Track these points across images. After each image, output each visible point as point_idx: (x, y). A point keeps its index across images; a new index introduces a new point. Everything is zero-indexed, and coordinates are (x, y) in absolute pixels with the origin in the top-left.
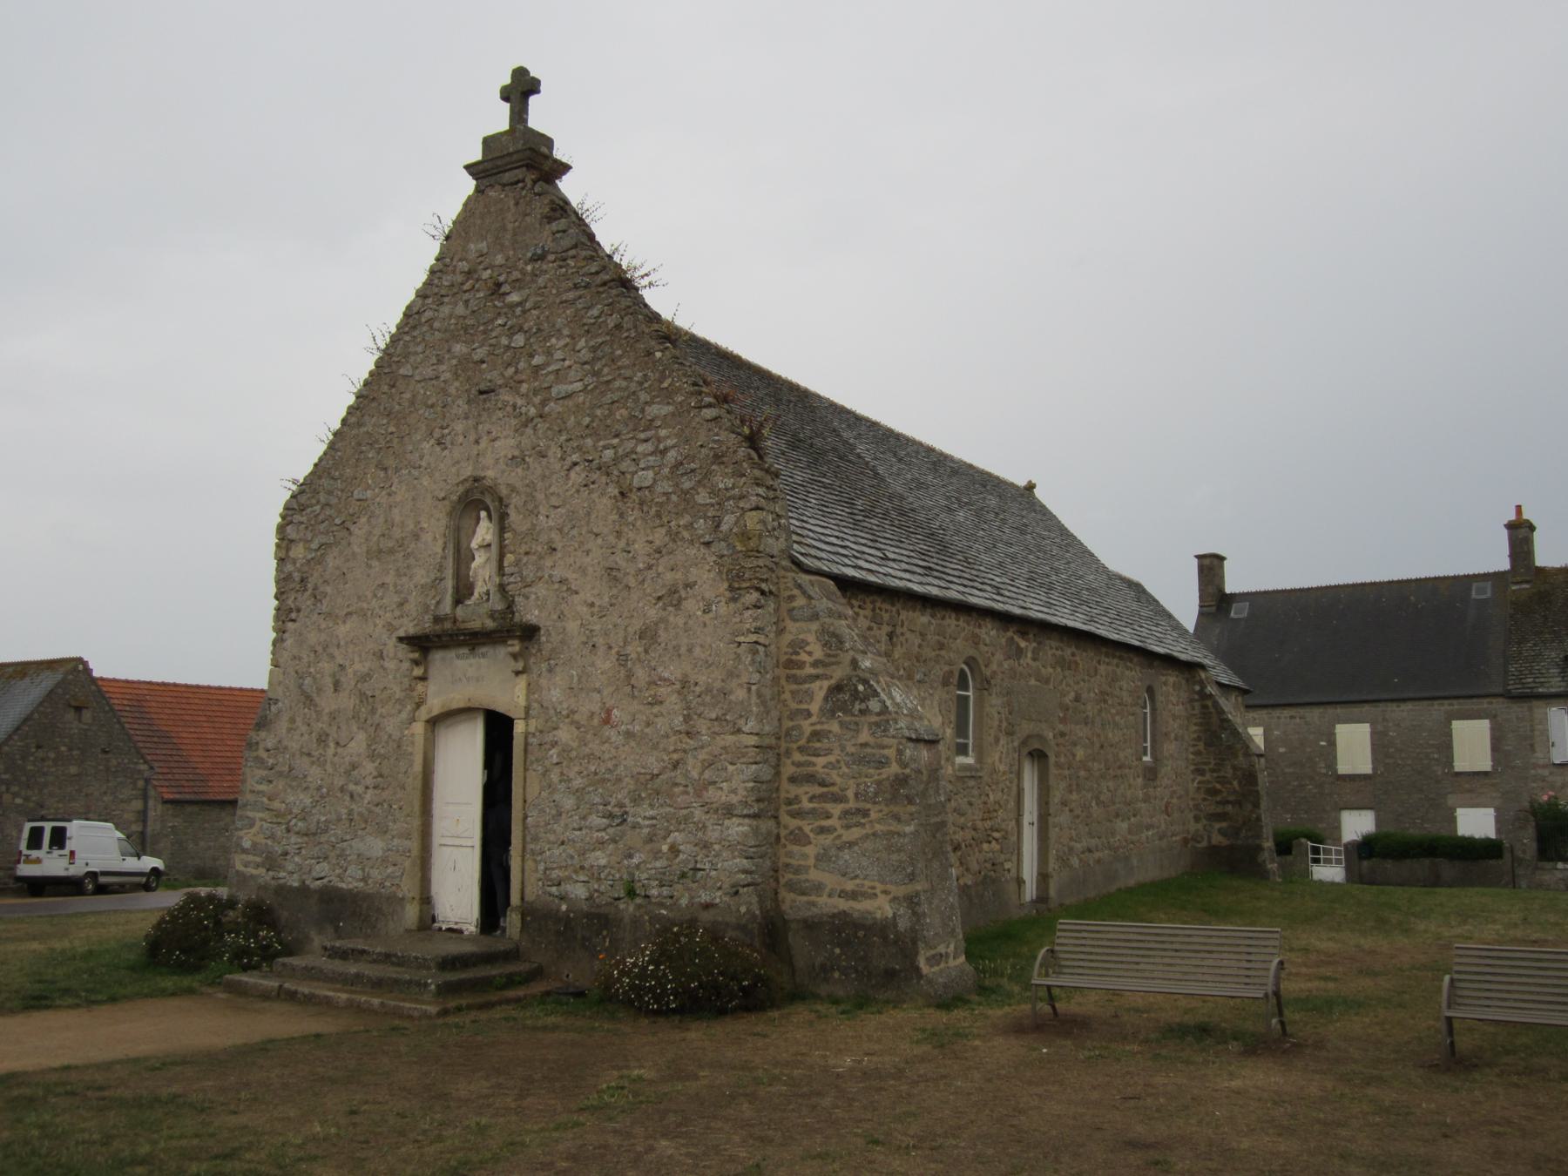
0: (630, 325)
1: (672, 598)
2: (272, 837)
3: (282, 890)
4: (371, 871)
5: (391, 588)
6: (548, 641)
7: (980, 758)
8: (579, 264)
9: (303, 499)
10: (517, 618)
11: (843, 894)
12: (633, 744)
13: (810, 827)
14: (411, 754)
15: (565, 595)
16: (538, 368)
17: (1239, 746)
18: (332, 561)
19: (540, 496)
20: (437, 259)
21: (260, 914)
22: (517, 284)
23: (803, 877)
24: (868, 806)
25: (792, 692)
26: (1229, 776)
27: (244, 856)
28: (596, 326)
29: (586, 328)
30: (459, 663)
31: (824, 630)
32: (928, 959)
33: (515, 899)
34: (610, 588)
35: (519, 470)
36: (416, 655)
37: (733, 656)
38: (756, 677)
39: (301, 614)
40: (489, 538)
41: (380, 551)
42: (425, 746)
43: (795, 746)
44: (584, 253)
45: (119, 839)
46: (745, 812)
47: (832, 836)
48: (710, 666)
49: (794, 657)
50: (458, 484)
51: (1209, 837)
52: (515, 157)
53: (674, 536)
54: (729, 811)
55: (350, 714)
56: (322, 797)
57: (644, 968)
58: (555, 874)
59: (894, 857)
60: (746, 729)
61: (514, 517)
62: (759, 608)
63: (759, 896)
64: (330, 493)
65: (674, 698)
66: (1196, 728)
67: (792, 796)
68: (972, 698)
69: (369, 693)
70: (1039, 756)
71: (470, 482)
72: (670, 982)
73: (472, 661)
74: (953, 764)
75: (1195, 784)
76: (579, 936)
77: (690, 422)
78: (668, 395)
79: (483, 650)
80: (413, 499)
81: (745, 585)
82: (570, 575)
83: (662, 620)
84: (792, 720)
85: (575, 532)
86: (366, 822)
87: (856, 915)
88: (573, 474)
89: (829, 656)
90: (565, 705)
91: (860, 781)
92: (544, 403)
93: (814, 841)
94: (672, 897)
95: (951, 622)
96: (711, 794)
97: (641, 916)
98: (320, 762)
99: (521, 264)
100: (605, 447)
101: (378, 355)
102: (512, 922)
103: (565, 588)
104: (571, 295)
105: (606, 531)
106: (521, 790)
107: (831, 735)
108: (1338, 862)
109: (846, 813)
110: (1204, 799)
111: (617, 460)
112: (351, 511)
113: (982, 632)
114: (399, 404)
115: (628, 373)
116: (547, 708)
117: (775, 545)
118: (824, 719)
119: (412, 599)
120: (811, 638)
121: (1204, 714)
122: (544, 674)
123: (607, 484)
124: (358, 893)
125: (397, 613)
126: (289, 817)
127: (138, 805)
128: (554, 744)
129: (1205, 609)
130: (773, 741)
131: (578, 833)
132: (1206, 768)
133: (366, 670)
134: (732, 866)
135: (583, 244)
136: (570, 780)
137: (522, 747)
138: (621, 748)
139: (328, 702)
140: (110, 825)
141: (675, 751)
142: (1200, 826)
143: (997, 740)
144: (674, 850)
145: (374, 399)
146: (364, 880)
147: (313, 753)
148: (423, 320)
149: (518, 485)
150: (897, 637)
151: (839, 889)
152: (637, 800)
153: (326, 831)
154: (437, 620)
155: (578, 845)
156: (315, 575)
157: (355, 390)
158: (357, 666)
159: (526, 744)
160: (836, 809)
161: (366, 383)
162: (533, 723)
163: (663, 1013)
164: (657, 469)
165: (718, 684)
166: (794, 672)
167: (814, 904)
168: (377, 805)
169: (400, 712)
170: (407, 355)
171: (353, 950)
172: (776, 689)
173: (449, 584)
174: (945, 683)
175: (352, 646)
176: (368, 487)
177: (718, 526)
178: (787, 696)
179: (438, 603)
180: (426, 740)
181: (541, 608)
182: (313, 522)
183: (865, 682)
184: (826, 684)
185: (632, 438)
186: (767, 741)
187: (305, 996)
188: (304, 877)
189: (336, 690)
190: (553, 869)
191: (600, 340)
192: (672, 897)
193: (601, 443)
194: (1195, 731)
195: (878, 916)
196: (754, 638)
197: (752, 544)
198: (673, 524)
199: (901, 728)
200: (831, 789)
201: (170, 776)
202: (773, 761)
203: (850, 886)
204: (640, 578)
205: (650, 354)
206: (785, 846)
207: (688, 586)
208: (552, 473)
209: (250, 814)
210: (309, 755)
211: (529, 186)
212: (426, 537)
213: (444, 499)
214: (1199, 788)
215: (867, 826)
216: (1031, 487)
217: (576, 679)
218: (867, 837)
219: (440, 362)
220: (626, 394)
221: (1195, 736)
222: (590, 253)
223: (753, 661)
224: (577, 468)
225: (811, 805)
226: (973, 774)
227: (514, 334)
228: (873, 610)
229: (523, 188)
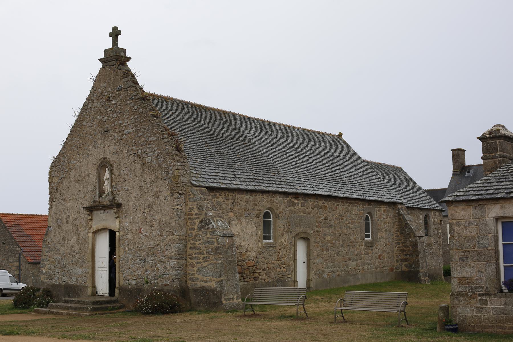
0: (145, 112)
1: (156, 195)
2: (50, 269)
3: (54, 286)
4: (78, 278)
5: (82, 192)
6: (124, 208)
7: (275, 240)
8: (131, 92)
9: (56, 163)
10: (116, 202)
11: (204, 281)
12: (147, 239)
14: (88, 243)
16: (120, 125)
17: (412, 233)
18: (65, 183)
19: (121, 164)
20: (92, 88)
21: (47, 293)
22: (115, 98)
23: (193, 277)
24: (209, 256)
25: (190, 223)
26: (408, 244)
27: (43, 276)
28: (136, 112)
29: (133, 112)
30: (101, 215)
31: (198, 205)
32: (225, 299)
33: (117, 285)
34: (141, 192)
35: (116, 156)
36: (89, 213)
37: (172, 213)
38: (178, 219)
39: (57, 200)
40: (108, 176)
41: (78, 180)
42: (92, 240)
43: (191, 238)
44: (132, 89)
45: (10, 276)
46: (175, 258)
47: (200, 265)
49: (190, 212)
50: (99, 160)
51: (402, 268)
52: (113, 58)
53: (157, 177)
54: (171, 258)
55: (71, 231)
56: (64, 256)
57: (144, 301)
58: (127, 277)
59: (216, 270)
60: (175, 234)
61: (115, 171)
62: (179, 198)
63: (179, 282)
64: (64, 161)
65: (157, 225)
66: (397, 227)
67: (190, 253)
68: (272, 220)
69: (77, 224)
70: (306, 239)
71: (103, 159)
72: (150, 305)
73: (105, 214)
74: (262, 242)
75: (397, 248)
76: (134, 295)
77: (161, 143)
78: (155, 134)
79: (107, 211)
80: (87, 164)
81: (175, 192)
82: (130, 189)
83: (154, 202)
84: (190, 231)
85: (131, 175)
86: (77, 264)
87: (206, 287)
88: (130, 158)
89: (199, 212)
90: (129, 227)
91: (207, 248)
92: (122, 135)
93: (196, 266)
94: (157, 283)
95: (260, 197)
96: (168, 253)
97: (150, 289)
98: (63, 246)
100: (139, 150)
101: (77, 118)
102: (117, 291)
103: (129, 192)
104: (129, 102)
105: (139, 175)
106: (118, 253)
107: (200, 235)
109: (204, 258)
110: (400, 254)
111: (142, 153)
112: (70, 168)
113: (275, 199)
114: (83, 134)
115: (144, 127)
117: (185, 179)
119: (87, 195)
120: (195, 207)
121: (400, 221)
122: (123, 218)
123: (139, 161)
124: (75, 285)
125: (84, 200)
126: (55, 263)
127: (17, 264)
128: (127, 239)
129: (455, 173)
130: (184, 237)
131: (133, 265)
132: (401, 242)
133: (75, 217)
134: (172, 274)
135: (132, 86)
136: (131, 250)
137: (118, 240)
138: (144, 240)
139: (65, 227)
140: (6, 271)
141: (158, 240)
142: (398, 264)
143: (283, 234)
144: (158, 269)
145: (76, 132)
146: (76, 281)
147: (61, 243)
148: (89, 107)
149: (116, 160)
150: (236, 203)
151: (202, 280)
152: (148, 255)
153: (66, 267)
154: (95, 202)
155: (133, 269)
156: (60, 187)
157: (70, 129)
158: (73, 216)
159: (119, 239)
160: (201, 257)
161: (73, 127)
162: (121, 232)
163: (148, 313)
164: (152, 157)
165: (168, 221)
166: (190, 217)
167: (196, 284)
168: (80, 259)
169: (85, 230)
170: (84, 119)
171: (70, 300)
172: (185, 222)
173: (97, 191)
174: (258, 216)
175: (71, 210)
176: (75, 160)
177: (168, 174)
178: (189, 224)
179: (95, 196)
180: (92, 238)
181: (122, 198)
182: (59, 171)
183: (208, 220)
184: (199, 220)
185: (146, 147)
186: (182, 237)
187: (55, 312)
188: (60, 281)
190: (127, 276)
191: (137, 116)
192: (157, 283)
193: (138, 148)
194: (396, 228)
195: (212, 287)
196: (177, 207)
197: (176, 180)
198: (156, 173)
199: (218, 233)
200: (200, 251)
201: (31, 253)
202: (184, 243)
203: (205, 279)
204: (148, 189)
205: (150, 121)
206: (188, 268)
207: (160, 192)
208: (125, 157)
209: (45, 263)
210: (60, 243)
211: (117, 67)
212: (91, 176)
213: (96, 164)
214: (398, 249)
215: (209, 261)
216: (340, 135)
217: (132, 219)
218: (209, 264)
219: (94, 121)
220: (144, 133)
221: (397, 229)
222: (134, 89)
223: (177, 214)
224: (131, 156)
225: (195, 256)
226: (271, 246)
227: (114, 113)
228: (225, 195)
229: (115, 67)
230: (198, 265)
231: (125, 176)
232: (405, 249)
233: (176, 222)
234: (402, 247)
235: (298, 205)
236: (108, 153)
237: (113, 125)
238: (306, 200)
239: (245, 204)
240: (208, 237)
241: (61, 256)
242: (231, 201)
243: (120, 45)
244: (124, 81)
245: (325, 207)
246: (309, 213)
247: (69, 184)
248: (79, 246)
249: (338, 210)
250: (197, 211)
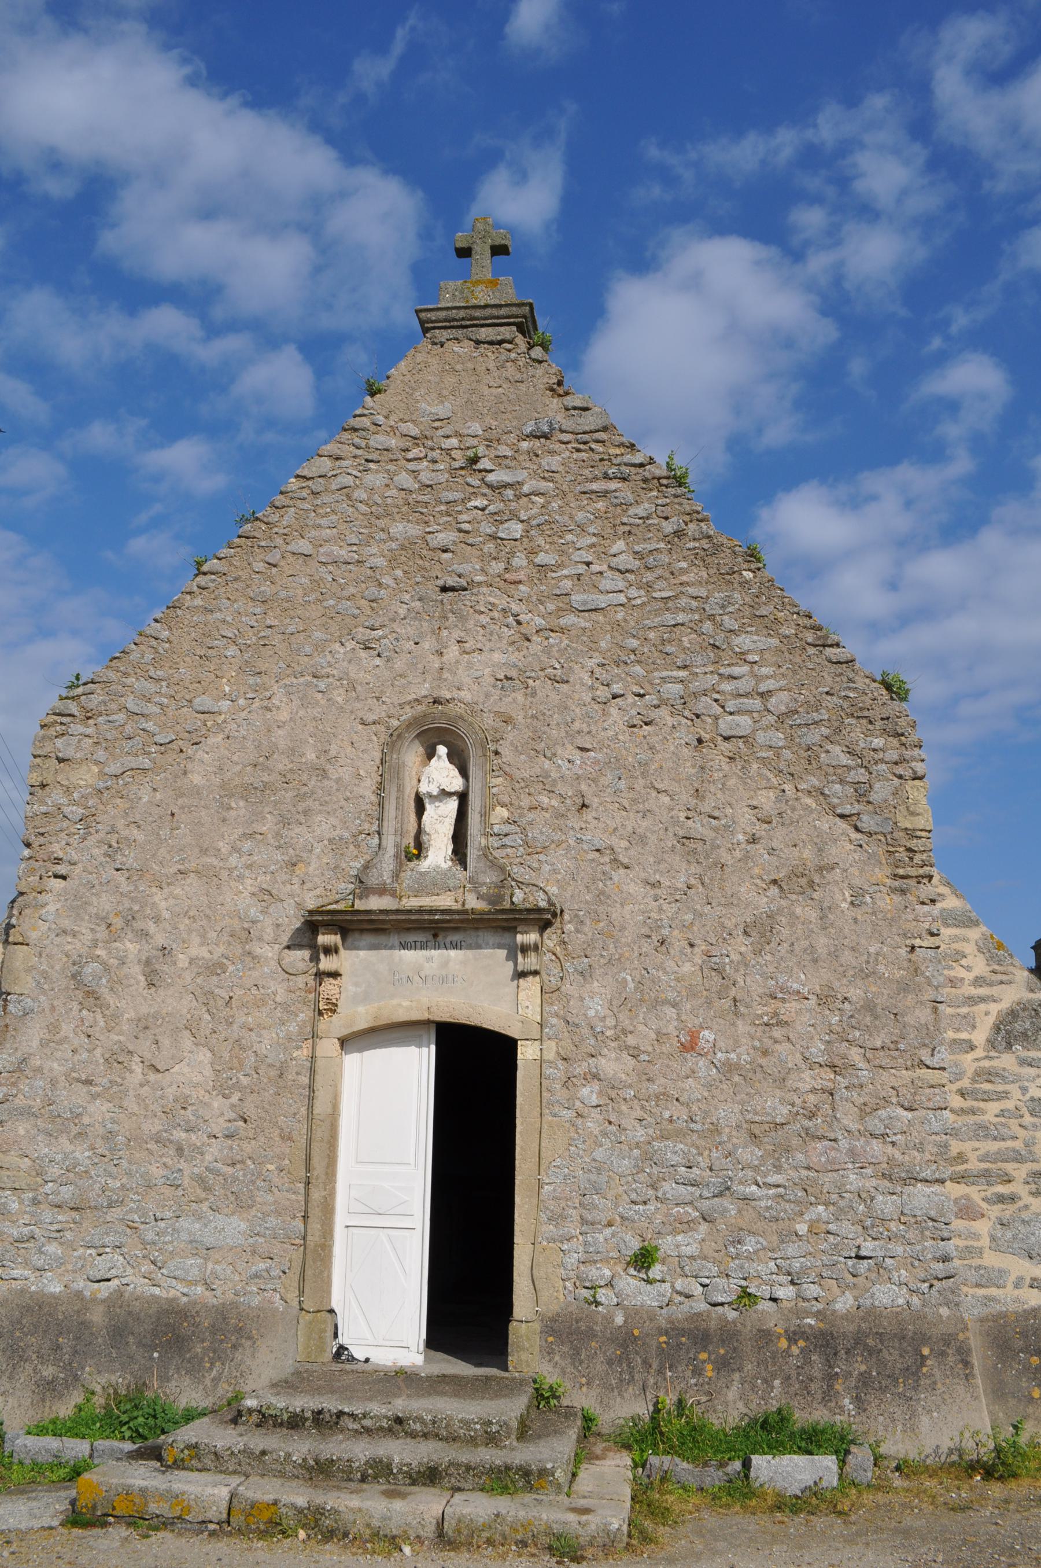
13: (983, 1194)
15: (607, 868)
48: (868, 976)
89: (994, 972)
99: (512, 438)
112: (189, 728)
116: (577, 1026)
118: (993, 1054)
120: (969, 948)
148: (334, 487)
184: (994, 1008)
189: (151, 985)
209: (208, 1272)
210: (88, 1082)
212: (340, 772)
247: (180, 801)
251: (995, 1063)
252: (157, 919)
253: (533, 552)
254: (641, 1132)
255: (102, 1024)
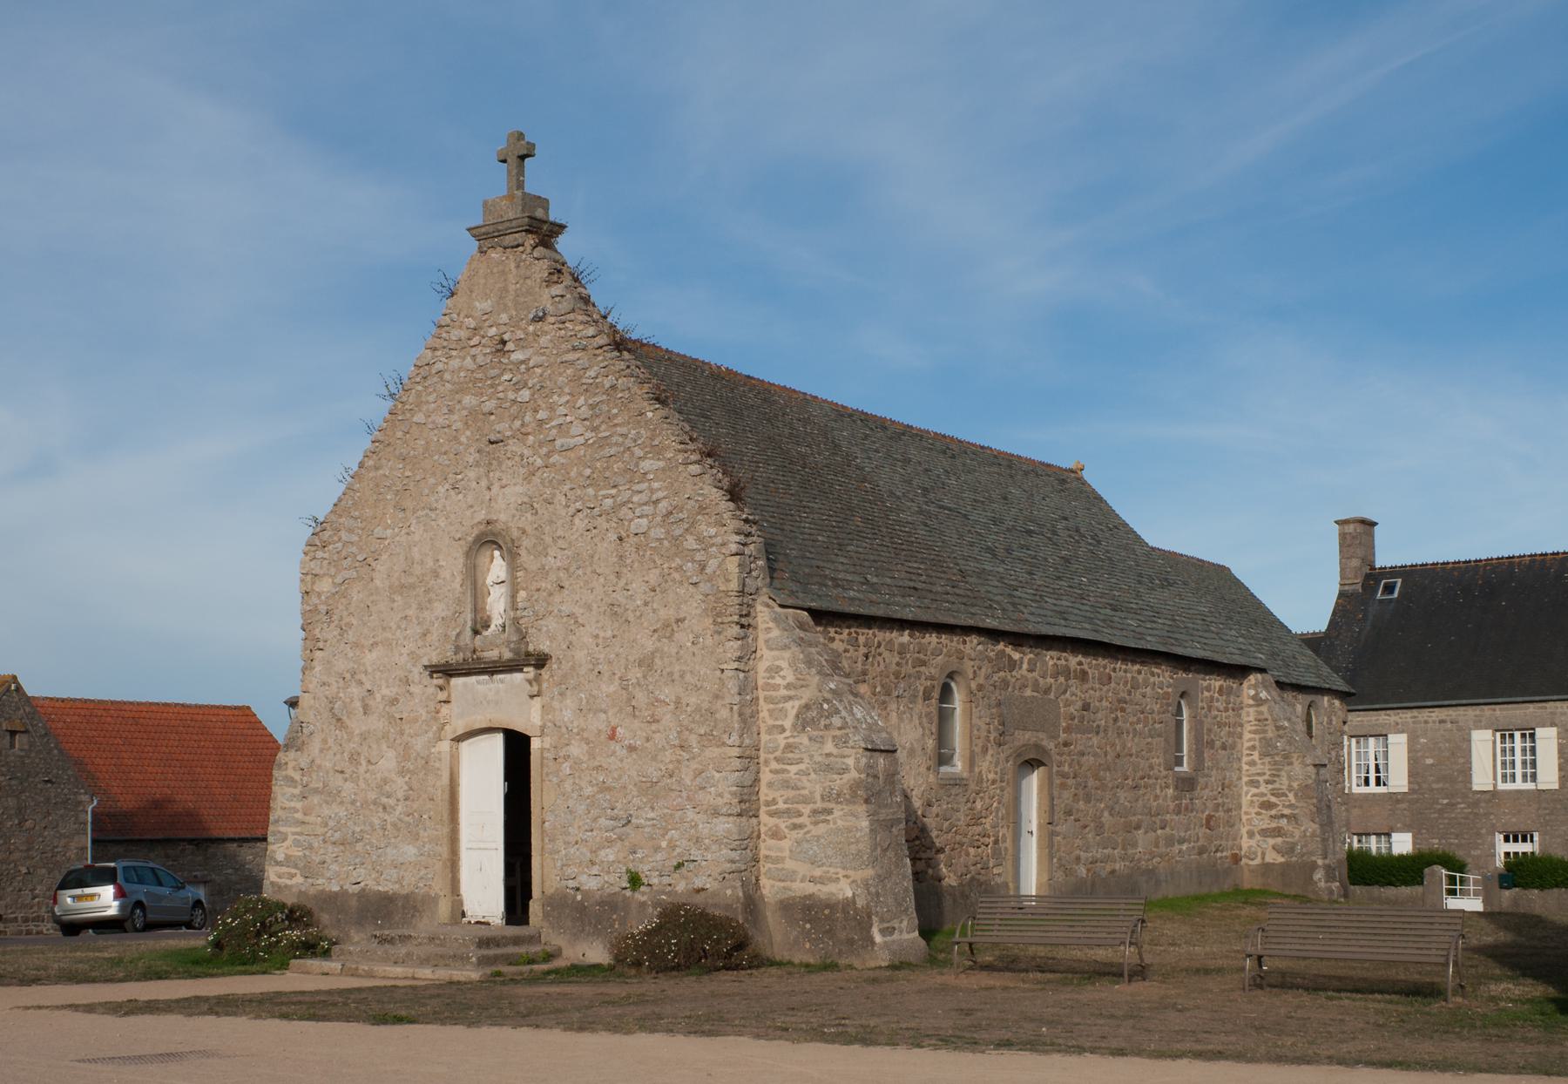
1: (667, 630)
5: (414, 620)
8: (577, 328)
16: (541, 422)
19: (548, 540)
25: (768, 710)
26: (1284, 787)
27: (278, 868)
47: (802, 832)
51: (1263, 854)
52: (514, 223)
67: (770, 798)
69: (398, 716)
75: (1249, 797)
78: (657, 451)
80: (431, 539)
82: (578, 611)
88: (577, 521)
90: (575, 724)
92: (548, 455)
93: (788, 836)
95: (932, 639)
102: (535, 907)
104: (570, 357)
108: (1476, 894)
112: (373, 550)
115: (623, 430)
120: (784, 664)
128: (567, 757)
131: (590, 834)
132: (1261, 779)
136: (581, 789)
138: (625, 760)
139: (358, 724)
154: (458, 649)
158: (385, 691)
159: (543, 758)
160: (806, 810)
165: (705, 705)
176: (387, 527)
184: (797, 703)
189: (365, 713)
191: (597, 399)
198: (665, 566)
203: (818, 872)
206: (764, 841)
209: (283, 829)
210: (342, 772)
212: (445, 574)
214: (1252, 802)
217: (584, 701)
219: (451, 411)
220: (622, 449)
225: (786, 806)
227: (519, 390)
230: (792, 832)
231: (562, 575)
232: (1273, 799)
233: (732, 708)
234: (1266, 795)
235: (1021, 668)
236: (504, 506)
237: (518, 423)
238: (1038, 654)
239: (897, 659)
240: (827, 752)
241: (347, 810)
242: (863, 650)
243: (531, 187)
244: (554, 294)
245: (1084, 673)
246: (1047, 691)
247: (371, 598)
248: (407, 779)
249: (1113, 685)
250: (790, 678)
251: (796, 740)
252: (366, 672)
253: (536, 411)
254: (590, 789)
255: (345, 737)
